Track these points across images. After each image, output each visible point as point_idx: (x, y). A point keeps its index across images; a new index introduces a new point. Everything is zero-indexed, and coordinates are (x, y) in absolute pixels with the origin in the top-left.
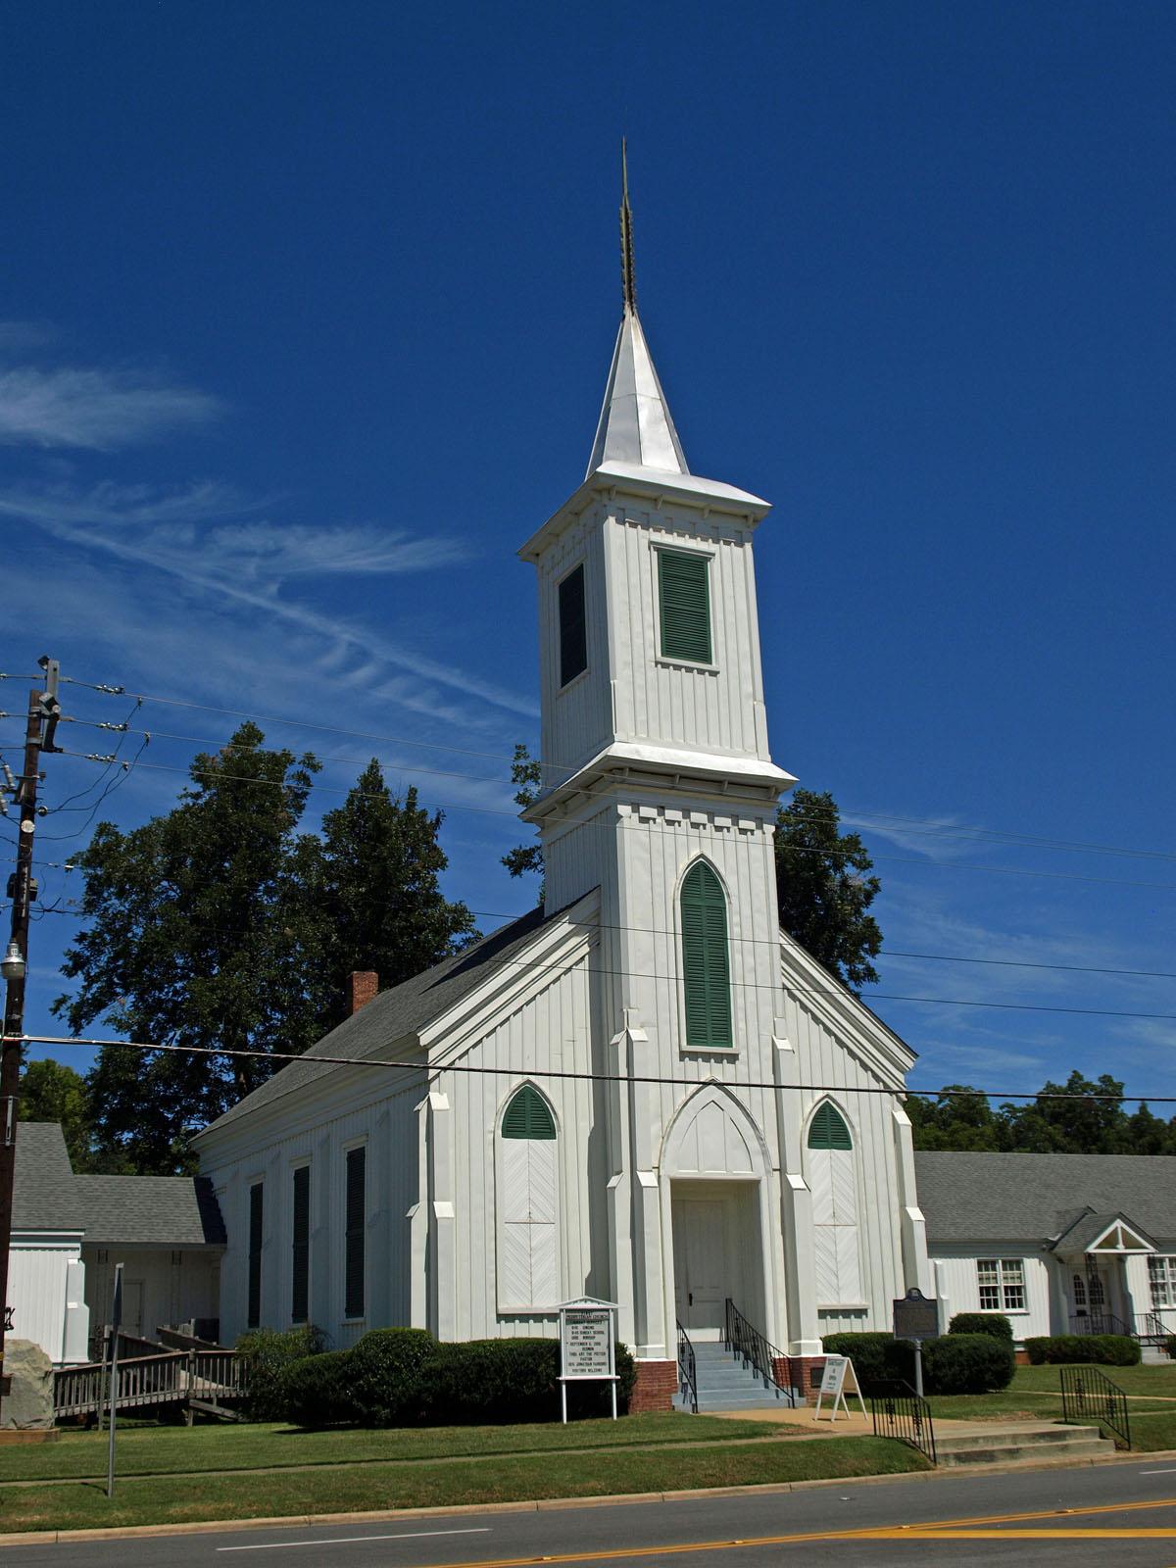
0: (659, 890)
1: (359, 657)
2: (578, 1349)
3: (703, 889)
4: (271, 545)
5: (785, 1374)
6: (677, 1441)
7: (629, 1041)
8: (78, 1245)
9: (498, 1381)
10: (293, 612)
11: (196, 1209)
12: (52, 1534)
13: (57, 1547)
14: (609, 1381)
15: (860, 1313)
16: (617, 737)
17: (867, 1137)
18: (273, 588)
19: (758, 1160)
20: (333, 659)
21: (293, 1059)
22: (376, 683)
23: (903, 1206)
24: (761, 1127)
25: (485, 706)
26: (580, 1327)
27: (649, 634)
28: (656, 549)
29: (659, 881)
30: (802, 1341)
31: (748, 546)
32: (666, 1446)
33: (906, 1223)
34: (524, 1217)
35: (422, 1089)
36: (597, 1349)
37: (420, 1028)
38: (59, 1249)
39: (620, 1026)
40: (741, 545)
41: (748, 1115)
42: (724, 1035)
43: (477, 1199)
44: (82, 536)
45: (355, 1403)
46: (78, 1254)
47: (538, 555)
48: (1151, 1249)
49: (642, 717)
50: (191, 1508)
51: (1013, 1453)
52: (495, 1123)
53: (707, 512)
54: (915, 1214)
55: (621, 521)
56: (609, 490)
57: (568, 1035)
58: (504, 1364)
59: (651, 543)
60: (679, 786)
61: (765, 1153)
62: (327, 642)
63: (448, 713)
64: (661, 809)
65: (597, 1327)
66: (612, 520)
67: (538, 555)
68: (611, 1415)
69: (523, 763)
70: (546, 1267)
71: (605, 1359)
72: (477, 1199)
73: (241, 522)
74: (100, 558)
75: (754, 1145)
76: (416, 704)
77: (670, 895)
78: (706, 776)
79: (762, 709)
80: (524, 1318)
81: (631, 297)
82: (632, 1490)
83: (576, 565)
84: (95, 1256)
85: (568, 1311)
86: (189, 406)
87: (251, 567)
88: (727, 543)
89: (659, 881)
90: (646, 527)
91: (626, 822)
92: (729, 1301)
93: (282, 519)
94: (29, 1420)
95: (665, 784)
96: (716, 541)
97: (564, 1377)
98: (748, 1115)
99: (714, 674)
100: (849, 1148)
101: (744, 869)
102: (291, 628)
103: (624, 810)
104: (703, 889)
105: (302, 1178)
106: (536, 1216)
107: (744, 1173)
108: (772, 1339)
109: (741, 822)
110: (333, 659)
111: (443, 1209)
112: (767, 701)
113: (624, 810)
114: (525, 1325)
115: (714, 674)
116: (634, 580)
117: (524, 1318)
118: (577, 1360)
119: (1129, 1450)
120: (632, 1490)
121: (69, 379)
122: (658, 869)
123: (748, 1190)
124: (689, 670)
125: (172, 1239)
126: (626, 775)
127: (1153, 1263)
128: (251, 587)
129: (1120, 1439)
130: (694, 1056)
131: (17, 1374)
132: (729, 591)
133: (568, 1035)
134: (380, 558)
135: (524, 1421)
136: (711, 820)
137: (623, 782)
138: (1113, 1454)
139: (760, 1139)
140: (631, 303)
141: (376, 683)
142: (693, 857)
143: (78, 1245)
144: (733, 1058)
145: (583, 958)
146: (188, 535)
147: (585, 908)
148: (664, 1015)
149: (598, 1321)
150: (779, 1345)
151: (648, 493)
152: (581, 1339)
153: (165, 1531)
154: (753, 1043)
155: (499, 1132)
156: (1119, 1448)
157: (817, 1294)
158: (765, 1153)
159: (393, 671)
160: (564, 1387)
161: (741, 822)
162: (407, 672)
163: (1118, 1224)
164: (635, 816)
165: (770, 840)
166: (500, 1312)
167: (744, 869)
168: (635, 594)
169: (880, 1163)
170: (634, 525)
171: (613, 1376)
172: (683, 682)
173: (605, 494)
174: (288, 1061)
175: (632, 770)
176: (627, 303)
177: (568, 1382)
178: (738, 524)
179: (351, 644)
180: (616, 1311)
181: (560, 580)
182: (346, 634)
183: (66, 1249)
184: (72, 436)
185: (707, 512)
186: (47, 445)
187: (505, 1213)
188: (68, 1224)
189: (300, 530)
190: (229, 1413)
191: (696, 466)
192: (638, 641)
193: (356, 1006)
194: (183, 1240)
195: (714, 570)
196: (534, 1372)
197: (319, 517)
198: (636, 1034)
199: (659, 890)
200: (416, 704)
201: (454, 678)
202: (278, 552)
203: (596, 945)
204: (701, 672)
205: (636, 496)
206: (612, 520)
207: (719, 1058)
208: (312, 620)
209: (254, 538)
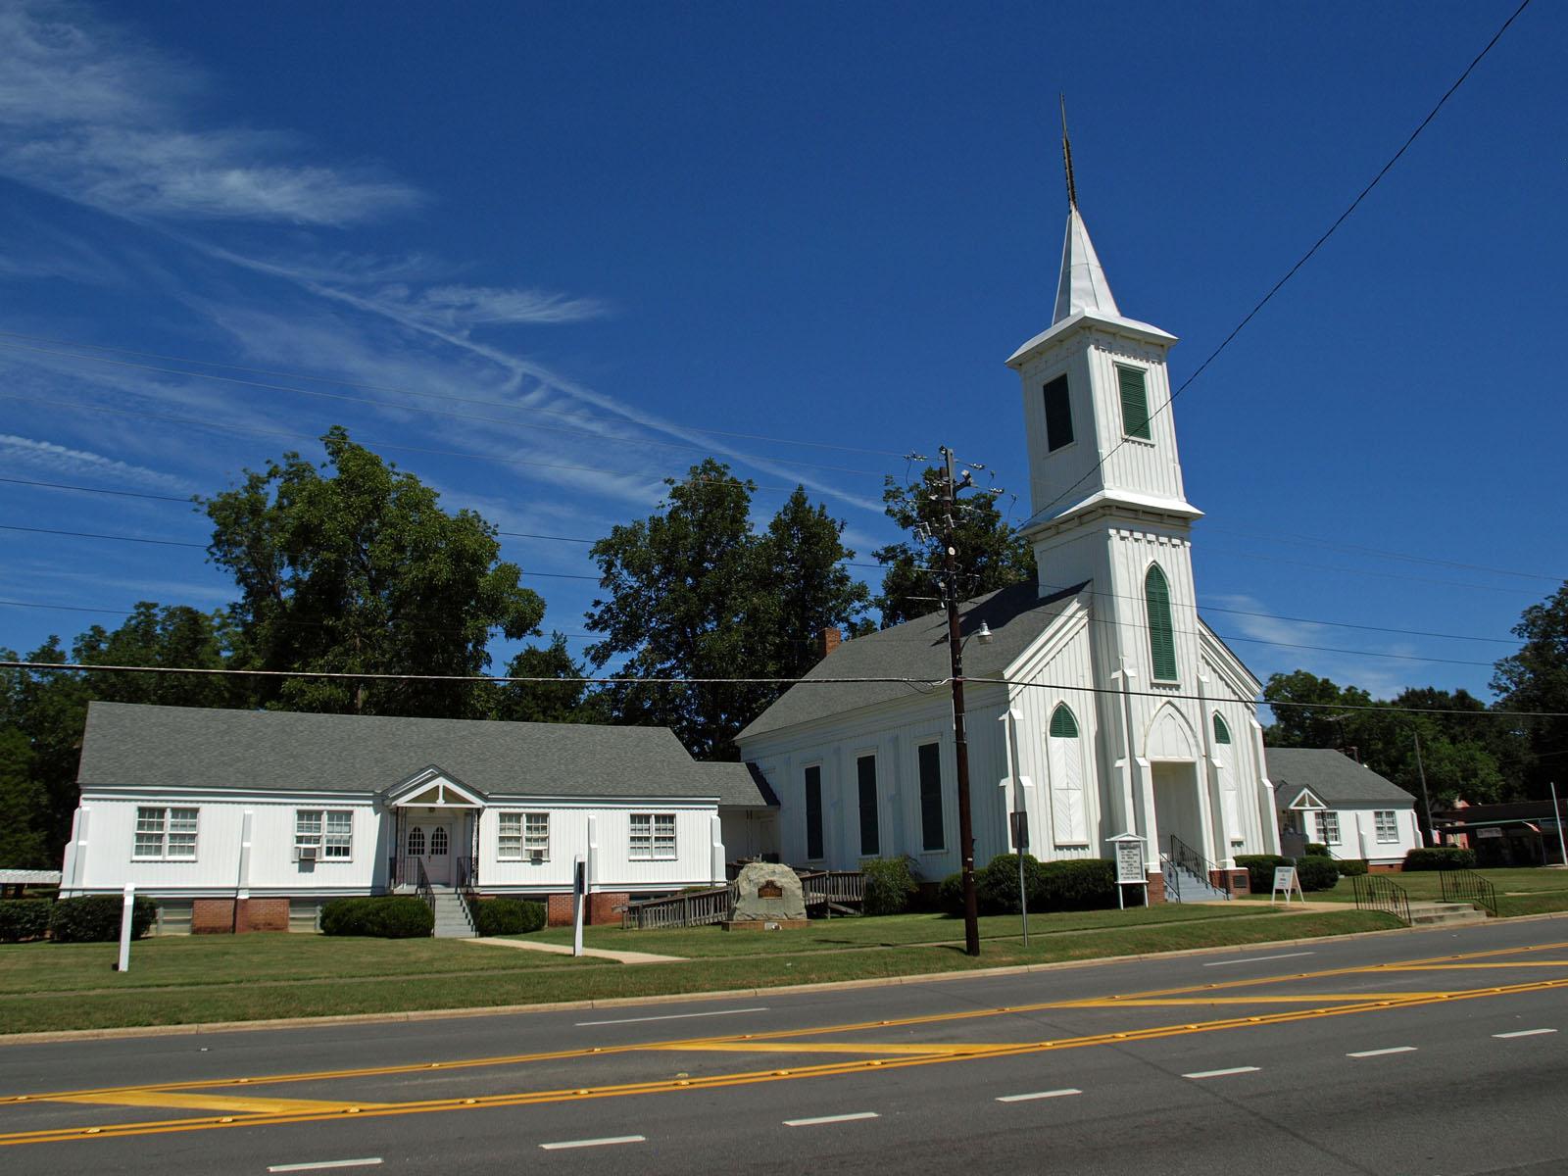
0: (1133, 582)
1: (530, 384)
2: (1125, 865)
3: (1155, 578)
4: (467, 300)
5: (1216, 880)
6: (947, 941)
7: (1125, 675)
8: (716, 806)
9: (1085, 885)
10: (484, 350)
11: (754, 783)
12: (1025, 967)
13: (1029, 973)
14: (1141, 885)
15: (1084, 847)
16: (1106, 486)
17: (1238, 736)
18: (466, 333)
19: (1194, 749)
20: (511, 386)
21: (794, 683)
22: (543, 403)
23: (1259, 778)
24: (1193, 727)
25: (625, 422)
26: (1126, 852)
27: (1117, 420)
28: (1117, 366)
29: (1132, 576)
30: (1150, 864)
31: (1164, 364)
32: (517, 971)
33: (1262, 788)
34: (1064, 786)
35: (1004, 704)
36: (1136, 865)
37: (1004, 668)
38: (705, 809)
39: (1117, 665)
40: (1160, 363)
41: (1188, 723)
42: (1172, 674)
43: (1040, 775)
44: (330, 292)
45: (999, 899)
46: (716, 812)
47: (1021, 365)
48: (1324, 807)
49: (1117, 474)
50: (991, 958)
51: (1441, 918)
52: (1046, 727)
53: (1142, 343)
54: (1268, 783)
55: (1097, 348)
56: (1089, 328)
57: (1080, 674)
58: (1088, 875)
59: (1114, 362)
60: (1114, 513)
61: (1198, 745)
62: (505, 373)
63: (597, 427)
64: (1131, 531)
65: (1135, 852)
66: (1092, 347)
67: (1021, 365)
68: (1119, 906)
69: (889, 487)
70: (1078, 816)
71: (1139, 871)
72: (1040, 775)
73: (444, 283)
74: (342, 309)
75: (1192, 741)
76: (573, 420)
77: (1139, 586)
78: (1124, 506)
79: (1178, 468)
80: (1068, 847)
81: (1074, 198)
82: (562, 997)
83: (1062, 373)
84: (724, 813)
85: (1120, 842)
86: (399, 195)
87: (450, 314)
88: (1153, 362)
89: (1132, 576)
90: (1110, 352)
91: (1113, 539)
92: (1173, 837)
93: (471, 282)
94: (794, 913)
95: (1133, 516)
96: (1148, 361)
97: (1121, 881)
98: (1188, 723)
99: (1152, 446)
100: (1229, 742)
101: (1176, 571)
102: (481, 362)
103: (1112, 532)
104: (1155, 578)
105: (867, 767)
106: (1071, 786)
107: (1186, 758)
108: (1207, 858)
109: (1122, 531)
110: (511, 386)
111: (1025, 781)
112: (1181, 463)
113: (1112, 532)
114: (1062, 852)
115: (1152, 446)
116: (1107, 385)
117: (1068, 847)
118: (1125, 871)
119: (1496, 916)
120: (457, 1005)
121: (313, 175)
122: (1132, 569)
123: (1189, 768)
124: (1140, 443)
125: (747, 803)
126: (1114, 511)
127: (1321, 816)
128: (451, 331)
129: (1489, 910)
130: (1158, 686)
131: (785, 886)
132: (1157, 394)
133: (1080, 674)
134: (548, 312)
135: (1079, 910)
136: (1170, 541)
137: (1111, 515)
138: (1484, 918)
139: (1195, 737)
140: (1075, 202)
141: (543, 403)
142: (1150, 562)
143: (716, 806)
144: (1177, 687)
145: (1085, 625)
146: (403, 292)
147: (1084, 593)
148: (1141, 661)
149: (1134, 848)
150: (1212, 863)
151: (1157, 342)
152: (1126, 859)
153: (352, 1021)
154: (1188, 678)
155: (1048, 733)
156: (1489, 915)
157: (1232, 832)
158: (1198, 745)
159: (556, 394)
160: (1120, 888)
161: (1122, 531)
162: (568, 396)
163: (1306, 791)
164: (1118, 537)
165: (1188, 549)
166: (1057, 844)
167: (1176, 571)
168: (1108, 394)
169: (1245, 752)
170: (1103, 351)
171: (1144, 881)
172: (1134, 450)
173: (1087, 330)
174: (788, 686)
175: (1117, 507)
176: (1072, 202)
177: (1123, 885)
178: (1159, 350)
179: (525, 376)
180: (1145, 843)
181: (1046, 382)
182: (520, 367)
183: (285, 804)
184: (314, 216)
185: (1142, 343)
186: (298, 223)
187: (1055, 784)
188: (710, 793)
189: (487, 291)
190: (851, 911)
191: (1124, 312)
192: (1111, 425)
193: (828, 651)
194: (754, 803)
195: (1147, 377)
196: (1103, 879)
197: (503, 282)
198: (1129, 673)
199: (1133, 582)
200: (573, 420)
201: (605, 402)
202: (471, 306)
203: (1092, 617)
204: (1146, 445)
205: (1128, 338)
206: (1092, 347)
207: (1171, 687)
208: (499, 356)
209: (455, 296)
